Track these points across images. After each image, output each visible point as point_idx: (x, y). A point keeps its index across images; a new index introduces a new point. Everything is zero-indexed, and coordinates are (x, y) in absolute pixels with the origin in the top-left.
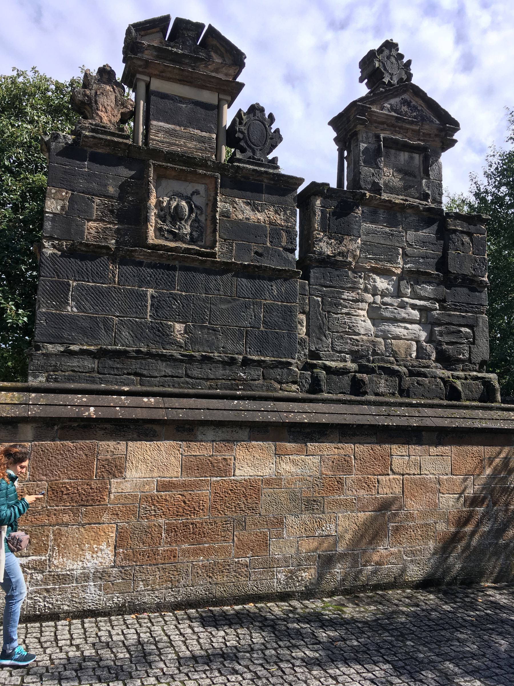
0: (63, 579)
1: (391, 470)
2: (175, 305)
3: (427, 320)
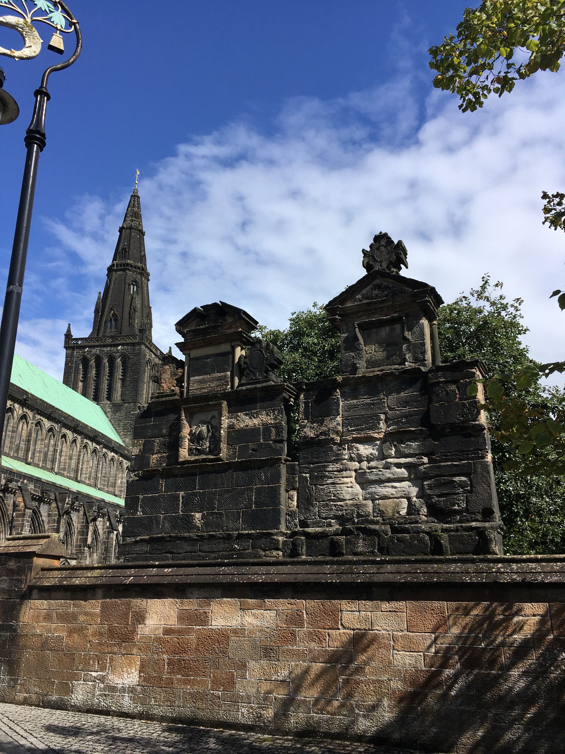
0: (113, 689)
1: (342, 624)
2: (196, 500)
3: (415, 475)
